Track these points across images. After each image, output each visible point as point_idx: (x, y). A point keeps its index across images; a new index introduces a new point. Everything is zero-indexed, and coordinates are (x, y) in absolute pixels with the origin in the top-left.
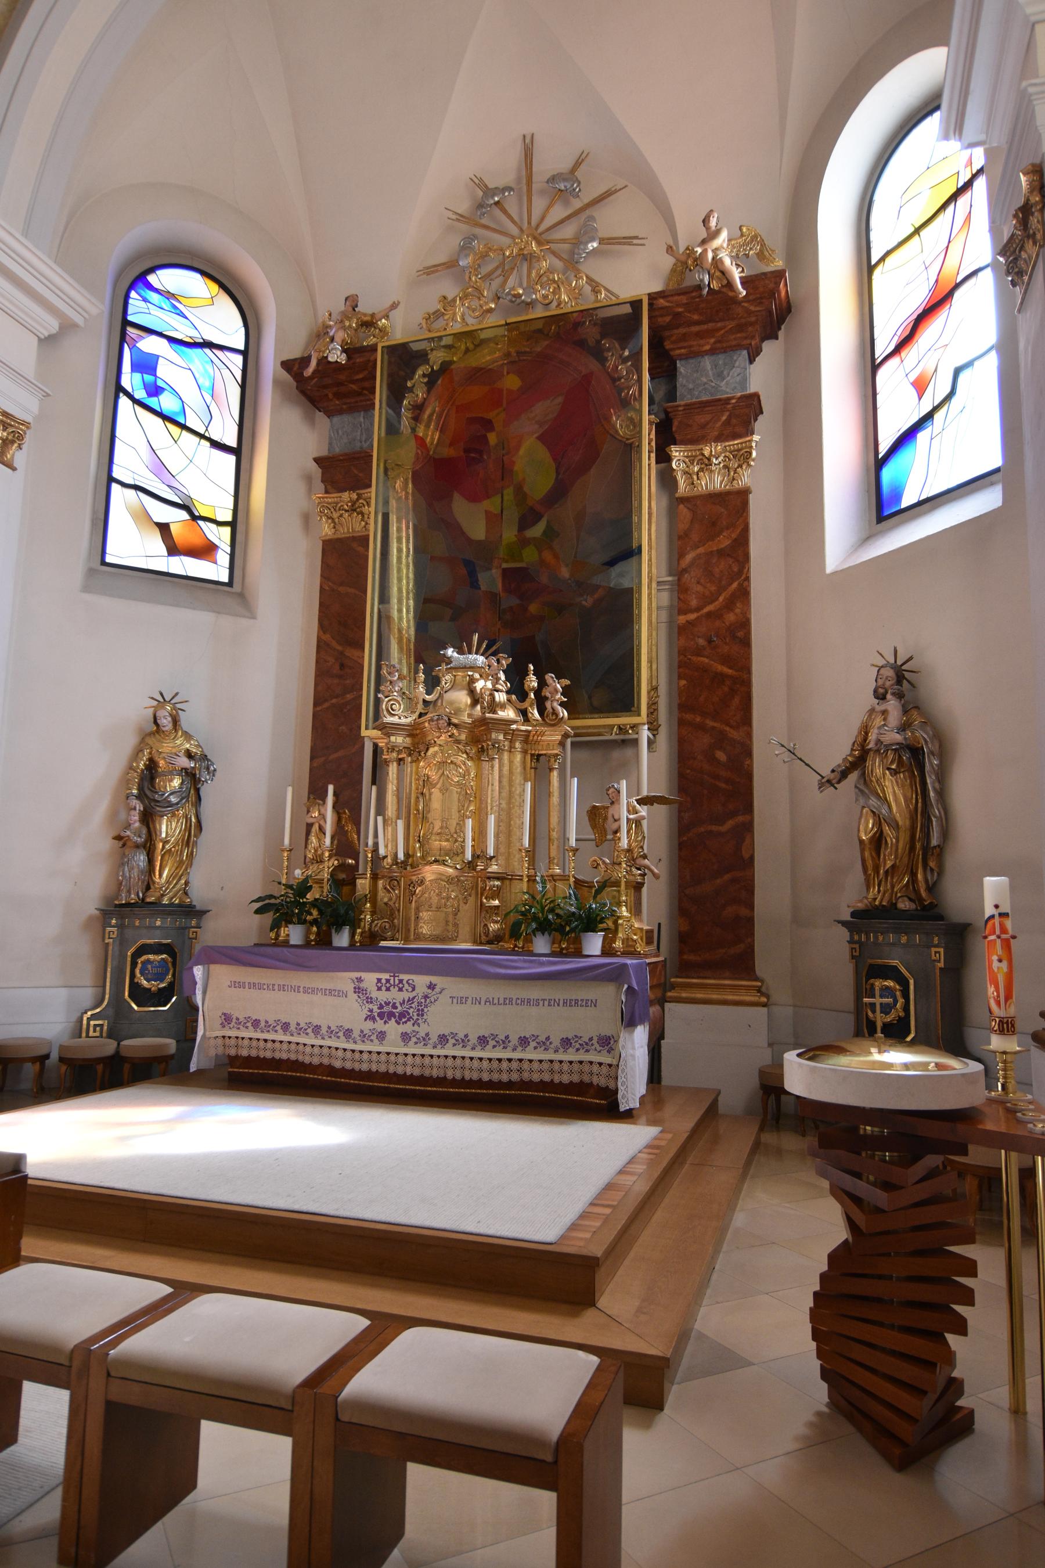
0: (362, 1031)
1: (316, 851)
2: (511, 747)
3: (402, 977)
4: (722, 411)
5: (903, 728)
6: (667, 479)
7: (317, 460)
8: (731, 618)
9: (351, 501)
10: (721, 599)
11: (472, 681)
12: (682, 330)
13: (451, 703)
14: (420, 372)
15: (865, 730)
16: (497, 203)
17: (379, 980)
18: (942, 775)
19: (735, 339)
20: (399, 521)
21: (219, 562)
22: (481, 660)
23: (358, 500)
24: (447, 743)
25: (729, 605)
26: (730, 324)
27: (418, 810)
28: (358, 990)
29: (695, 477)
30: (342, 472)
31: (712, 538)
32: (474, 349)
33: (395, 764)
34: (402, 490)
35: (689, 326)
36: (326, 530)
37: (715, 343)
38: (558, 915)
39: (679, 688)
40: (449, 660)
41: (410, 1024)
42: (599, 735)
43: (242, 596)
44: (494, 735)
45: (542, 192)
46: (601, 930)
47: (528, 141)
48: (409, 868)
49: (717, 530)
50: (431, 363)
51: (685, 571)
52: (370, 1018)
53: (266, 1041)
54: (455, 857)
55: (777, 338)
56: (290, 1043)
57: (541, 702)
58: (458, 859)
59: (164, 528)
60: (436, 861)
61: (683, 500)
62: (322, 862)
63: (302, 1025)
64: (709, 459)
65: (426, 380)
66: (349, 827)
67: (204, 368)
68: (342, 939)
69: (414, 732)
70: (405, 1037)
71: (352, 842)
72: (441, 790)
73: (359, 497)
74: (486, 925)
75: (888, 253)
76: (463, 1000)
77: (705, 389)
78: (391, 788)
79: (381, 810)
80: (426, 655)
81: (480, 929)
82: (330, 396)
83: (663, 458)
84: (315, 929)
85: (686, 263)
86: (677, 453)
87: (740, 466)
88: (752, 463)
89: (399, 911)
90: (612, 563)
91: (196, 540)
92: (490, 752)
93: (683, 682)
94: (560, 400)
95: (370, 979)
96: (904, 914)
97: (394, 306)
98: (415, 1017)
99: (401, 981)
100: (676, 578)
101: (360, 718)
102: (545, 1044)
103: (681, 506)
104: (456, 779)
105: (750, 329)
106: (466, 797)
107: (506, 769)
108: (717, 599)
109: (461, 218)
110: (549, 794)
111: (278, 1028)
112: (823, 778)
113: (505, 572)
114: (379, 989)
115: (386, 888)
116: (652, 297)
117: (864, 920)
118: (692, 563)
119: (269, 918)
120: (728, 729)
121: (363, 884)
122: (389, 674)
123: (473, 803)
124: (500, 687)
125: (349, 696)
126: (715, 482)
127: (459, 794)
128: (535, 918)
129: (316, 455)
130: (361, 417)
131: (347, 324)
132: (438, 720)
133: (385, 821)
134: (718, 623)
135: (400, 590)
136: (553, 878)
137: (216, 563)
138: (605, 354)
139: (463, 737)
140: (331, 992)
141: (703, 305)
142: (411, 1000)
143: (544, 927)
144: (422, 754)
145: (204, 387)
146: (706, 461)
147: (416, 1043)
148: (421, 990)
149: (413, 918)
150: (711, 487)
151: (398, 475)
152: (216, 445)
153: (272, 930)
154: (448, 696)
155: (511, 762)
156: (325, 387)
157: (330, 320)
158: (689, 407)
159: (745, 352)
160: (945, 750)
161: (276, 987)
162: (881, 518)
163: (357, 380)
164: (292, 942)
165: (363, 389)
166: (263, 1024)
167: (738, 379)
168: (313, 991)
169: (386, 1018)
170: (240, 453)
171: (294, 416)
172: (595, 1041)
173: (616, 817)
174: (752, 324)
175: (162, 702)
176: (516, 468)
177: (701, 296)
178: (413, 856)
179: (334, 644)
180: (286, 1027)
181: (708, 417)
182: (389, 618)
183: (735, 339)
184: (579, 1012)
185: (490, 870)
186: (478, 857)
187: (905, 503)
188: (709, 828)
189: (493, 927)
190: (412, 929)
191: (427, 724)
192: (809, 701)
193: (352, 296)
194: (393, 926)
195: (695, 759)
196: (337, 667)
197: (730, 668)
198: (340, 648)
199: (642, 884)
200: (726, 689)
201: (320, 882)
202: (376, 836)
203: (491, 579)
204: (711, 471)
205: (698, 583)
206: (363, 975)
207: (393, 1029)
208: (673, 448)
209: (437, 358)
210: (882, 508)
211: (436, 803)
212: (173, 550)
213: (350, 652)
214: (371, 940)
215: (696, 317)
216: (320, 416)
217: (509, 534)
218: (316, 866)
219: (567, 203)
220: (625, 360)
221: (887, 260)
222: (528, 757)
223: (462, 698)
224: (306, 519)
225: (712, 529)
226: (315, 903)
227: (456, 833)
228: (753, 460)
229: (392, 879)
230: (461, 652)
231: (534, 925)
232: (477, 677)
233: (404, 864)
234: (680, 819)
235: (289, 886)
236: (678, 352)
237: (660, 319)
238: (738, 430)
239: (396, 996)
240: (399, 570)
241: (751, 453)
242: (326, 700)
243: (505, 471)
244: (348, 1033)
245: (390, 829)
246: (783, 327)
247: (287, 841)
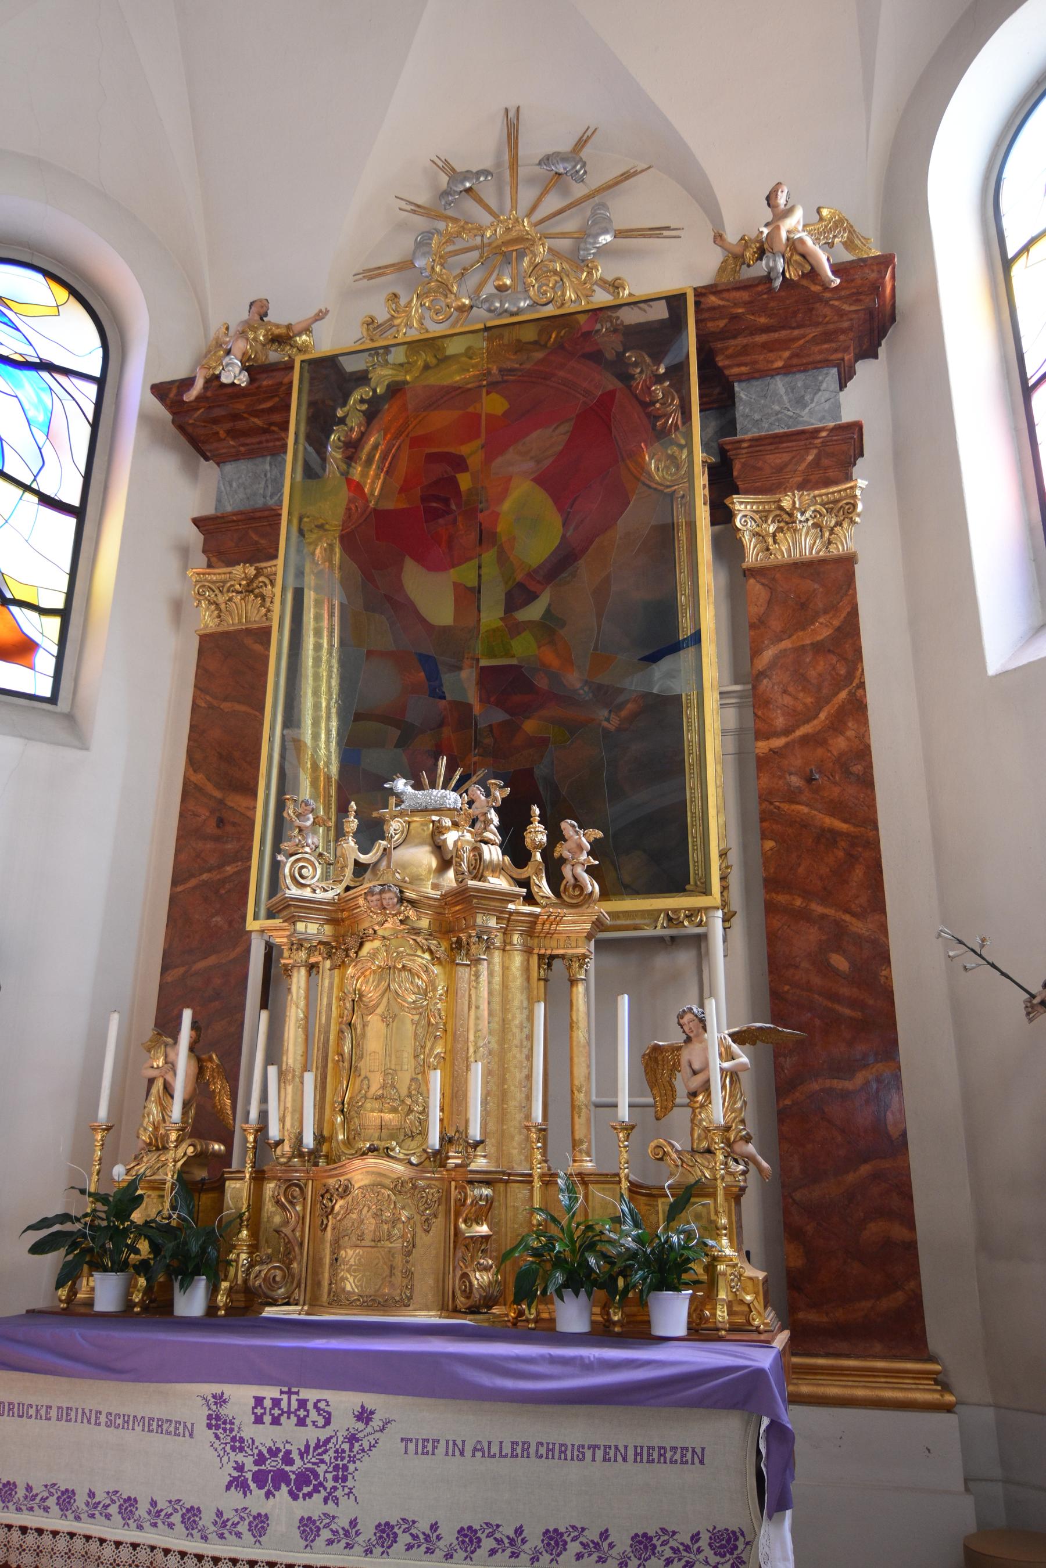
0: (219, 1514)
1: (156, 1128)
2: (505, 943)
3: (306, 1394)
4: (807, 449)
6: (728, 545)
7: (197, 522)
8: (840, 744)
9: (246, 578)
10: (822, 716)
11: (438, 830)
12: (741, 341)
13: (404, 866)
14: (356, 396)
16: (468, 190)
17: (259, 1401)
19: (821, 352)
20: (318, 603)
21: (37, 668)
22: (452, 798)
23: (256, 576)
24: (396, 933)
25: (837, 724)
26: (812, 332)
27: (341, 1055)
28: (215, 1422)
29: (770, 540)
30: (234, 538)
31: (802, 626)
32: (437, 365)
33: (303, 971)
34: (324, 562)
35: (752, 334)
36: (206, 620)
37: (790, 358)
38: (604, 1256)
39: (764, 854)
40: (400, 799)
41: (318, 1498)
42: (636, 928)
43: (70, 718)
44: (479, 919)
45: (531, 181)
46: (687, 1285)
47: (511, 114)
48: (322, 1162)
49: (810, 617)
50: (373, 384)
51: (762, 674)
52: (238, 1483)
53: (24, 1530)
54: (408, 1141)
55: (876, 357)
56: (72, 1535)
57: (554, 870)
58: (413, 1144)
60: (373, 1149)
62: (165, 1148)
63: (100, 1496)
64: (790, 515)
65: (365, 407)
66: (218, 1085)
67: (38, 396)
68: (192, 1302)
69: (339, 916)
70: (308, 1528)
71: (222, 1111)
72: (383, 1018)
73: (259, 572)
74: (465, 1275)
75: (1033, 241)
76: (426, 1447)
77: (778, 420)
78: (294, 1014)
79: (273, 1056)
80: (360, 789)
81: (454, 1282)
82: (222, 434)
83: (722, 515)
84: (142, 1282)
85: (743, 256)
86: (742, 506)
87: (839, 524)
88: (857, 519)
89: (301, 1244)
90: (654, 658)
92: (473, 949)
93: (770, 844)
94: (566, 428)
95: (240, 1396)
97: (320, 316)
98: (330, 1484)
99: (302, 1403)
100: (750, 687)
101: (245, 904)
103: (752, 581)
104: (411, 998)
105: (842, 337)
106: (428, 1029)
107: (497, 979)
108: (816, 716)
109: (418, 209)
110: (572, 1026)
111: (51, 1502)
112: (1033, 996)
113: (487, 675)
114: (259, 1420)
115: (278, 1202)
116: (700, 293)
118: (773, 665)
119: (52, 1261)
120: (847, 918)
121: (237, 1191)
122: (299, 816)
123: (441, 1042)
124: (491, 836)
125: (229, 869)
126: (805, 545)
127: (416, 1024)
128: (559, 1262)
129: (196, 515)
130: (265, 465)
131: (251, 336)
132: (381, 892)
133: (281, 1074)
134: (820, 752)
135: (317, 706)
136: (584, 1179)
137: (32, 668)
138: (631, 371)
139: (424, 923)
140: (159, 1426)
141: (772, 304)
142: (322, 1445)
143: (578, 1280)
144: (352, 954)
146: (786, 517)
147: (330, 1542)
148: (343, 1422)
149: (327, 1261)
150: (796, 555)
151: (319, 539)
152: (46, 500)
153: (59, 1285)
154: (398, 855)
155: (505, 968)
156: (216, 421)
157: (227, 335)
158: (757, 441)
159: (834, 371)
161: (53, 1413)
163: (263, 411)
164: (100, 1307)
165: (271, 424)
166: (21, 1492)
167: (827, 406)
168: (127, 1422)
169: (269, 1485)
171: (167, 466)
172: (704, 1543)
173: (696, 1066)
174: (843, 331)
176: (498, 530)
177: (770, 290)
178: (330, 1139)
179: (210, 788)
180: (66, 1499)
181: (786, 457)
182: (298, 743)
183: (821, 352)
184: (668, 1474)
185: (473, 1167)
186: (450, 1141)
188: (828, 1083)
189: (480, 1279)
190: (325, 1284)
191: (361, 901)
193: (261, 300)
194: (289, 1275)
195: (797, 967)
196: (213, 822)
197: (845, 821)
198: (218, 794)
199: (743, 1189)
200: (841, 854)
201: (158, 1186)
202: (264, 1099)
203: (464, 684)
204: (795, 530)
205: (785, 692)
206: (229, 1390)
207: (283, 1509)
208: (736, 498)
209: (382, 377)
213: (236, 801)
214: (244, 1309)
215: (763, 320)
217: (491, 616)
218: (153, 1157)
219: (565, 192)
220: (659, 379)
221: (1032, 250)
222: (534, 960)
223: (423, 858)
224: (177, 607)
225: (802, 612)
226: (146, 1229)
227: (410, 1096)
228: (859, 515)
229: (290, 1184)
230: (418, 786)
231: (559, 1277)
232: (442, 828)
233: (314, 1154)
234: (778, 1068)
235: (97, 1197)
236: (735, 370)
237: (710, 324)
238: (831, 474)
239: (291, 1436)
240: (317, 677)
241: (854, 506)
242: (193, 876)
244: (191, 1516)
245: (290, 1089)
246: (883, 342)
247: (103, 1113)
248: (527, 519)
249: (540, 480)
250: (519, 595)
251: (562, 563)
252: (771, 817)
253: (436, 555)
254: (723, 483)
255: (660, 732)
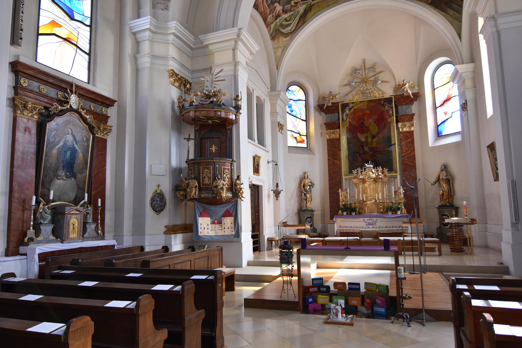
5: (446, 176)
8: (412, 154)
15: (439, 176)
17: (59, 234)
18: (453, 184)
25: (411, 152)
30: (331, 126)
43: (310, 150)
49: (408, 138)
59: (296, 138)
61: (401, 132)
83: (397, 123)
91: (301, 140)
95: (366, 219)
96: (448, 206)
102: (396, 227)
117: (440, 207)
145: (299, 109)
152: (302, 120)
160: (453, 179)
162: (439, 136)
170: (307, 121)
175: (305, 173)
187: (443, 134)
192: (428, 169)
207: (371, 226)
209: (351, 105)
210: (439, 135)
211: (368, 191)
212: (298, 142)
216: (323, 113)
225: (407, 138)
243: (368, 130)
244: (363, 228)
248: (374, 129)
249: (375, 122)
250: (373, 137)
251: (378, 133)
252: (403, 163)
253: (362, 132)
254: (397, 122)
255: (390, 154)
